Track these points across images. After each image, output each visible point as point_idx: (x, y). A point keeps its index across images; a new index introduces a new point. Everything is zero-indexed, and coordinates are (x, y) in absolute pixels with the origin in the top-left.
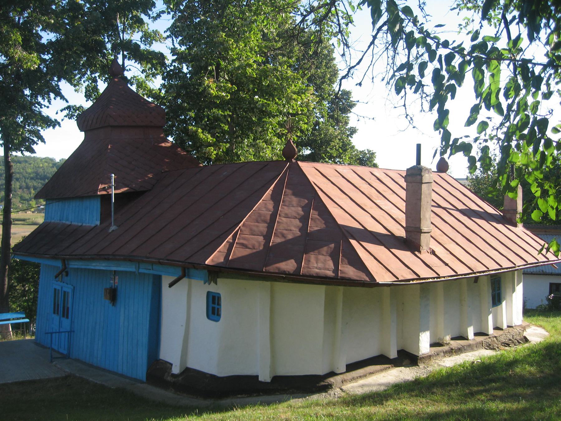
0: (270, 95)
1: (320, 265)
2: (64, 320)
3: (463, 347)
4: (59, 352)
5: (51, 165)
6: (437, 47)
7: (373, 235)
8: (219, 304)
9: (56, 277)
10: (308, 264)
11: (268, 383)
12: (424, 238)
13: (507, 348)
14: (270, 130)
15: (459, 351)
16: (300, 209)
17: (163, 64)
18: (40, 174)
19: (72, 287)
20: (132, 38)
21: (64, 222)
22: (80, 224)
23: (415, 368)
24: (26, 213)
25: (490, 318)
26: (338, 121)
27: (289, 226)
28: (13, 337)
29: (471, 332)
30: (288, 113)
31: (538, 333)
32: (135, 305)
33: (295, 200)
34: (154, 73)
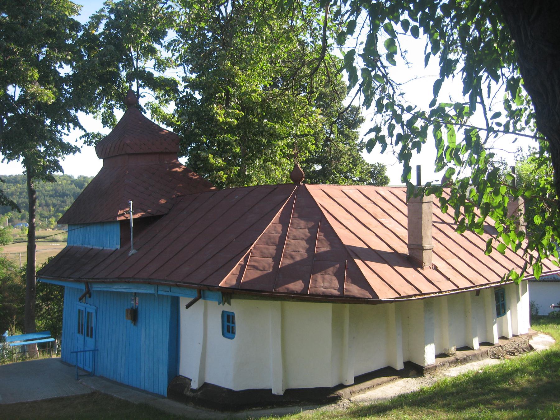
0: (279, 118)
1: (326, 284)
2: (88, 339)
3: (468, 356)
4: (84, 370)
5: (69, 182)
6: (402, 112)
7: (377, 254)
8: (233, 323)
9: (80, 299)
10: (316, 284)
11: (281, 396)
12: (426, 255)
13: (512, 357)
14: (279, 152)
15: (464, 361)
16: (307, 230)
17: (176, 91)
18: (59, 191)
19: (95, 308)
20: (146, 66)
21: (86, 246)
22: (101, 248)
23: (421, 379)
24: (46, 230)
25: (495, 327)
26: (347, 137)
27: (296, 249)
28: (40, 356)
29: (476, 343)
30: (296, 135)
31: (544, 341)
32: (154, 325)
33: (302, 223)
34: (167, 99)
